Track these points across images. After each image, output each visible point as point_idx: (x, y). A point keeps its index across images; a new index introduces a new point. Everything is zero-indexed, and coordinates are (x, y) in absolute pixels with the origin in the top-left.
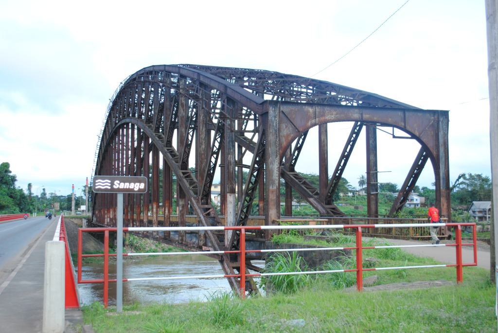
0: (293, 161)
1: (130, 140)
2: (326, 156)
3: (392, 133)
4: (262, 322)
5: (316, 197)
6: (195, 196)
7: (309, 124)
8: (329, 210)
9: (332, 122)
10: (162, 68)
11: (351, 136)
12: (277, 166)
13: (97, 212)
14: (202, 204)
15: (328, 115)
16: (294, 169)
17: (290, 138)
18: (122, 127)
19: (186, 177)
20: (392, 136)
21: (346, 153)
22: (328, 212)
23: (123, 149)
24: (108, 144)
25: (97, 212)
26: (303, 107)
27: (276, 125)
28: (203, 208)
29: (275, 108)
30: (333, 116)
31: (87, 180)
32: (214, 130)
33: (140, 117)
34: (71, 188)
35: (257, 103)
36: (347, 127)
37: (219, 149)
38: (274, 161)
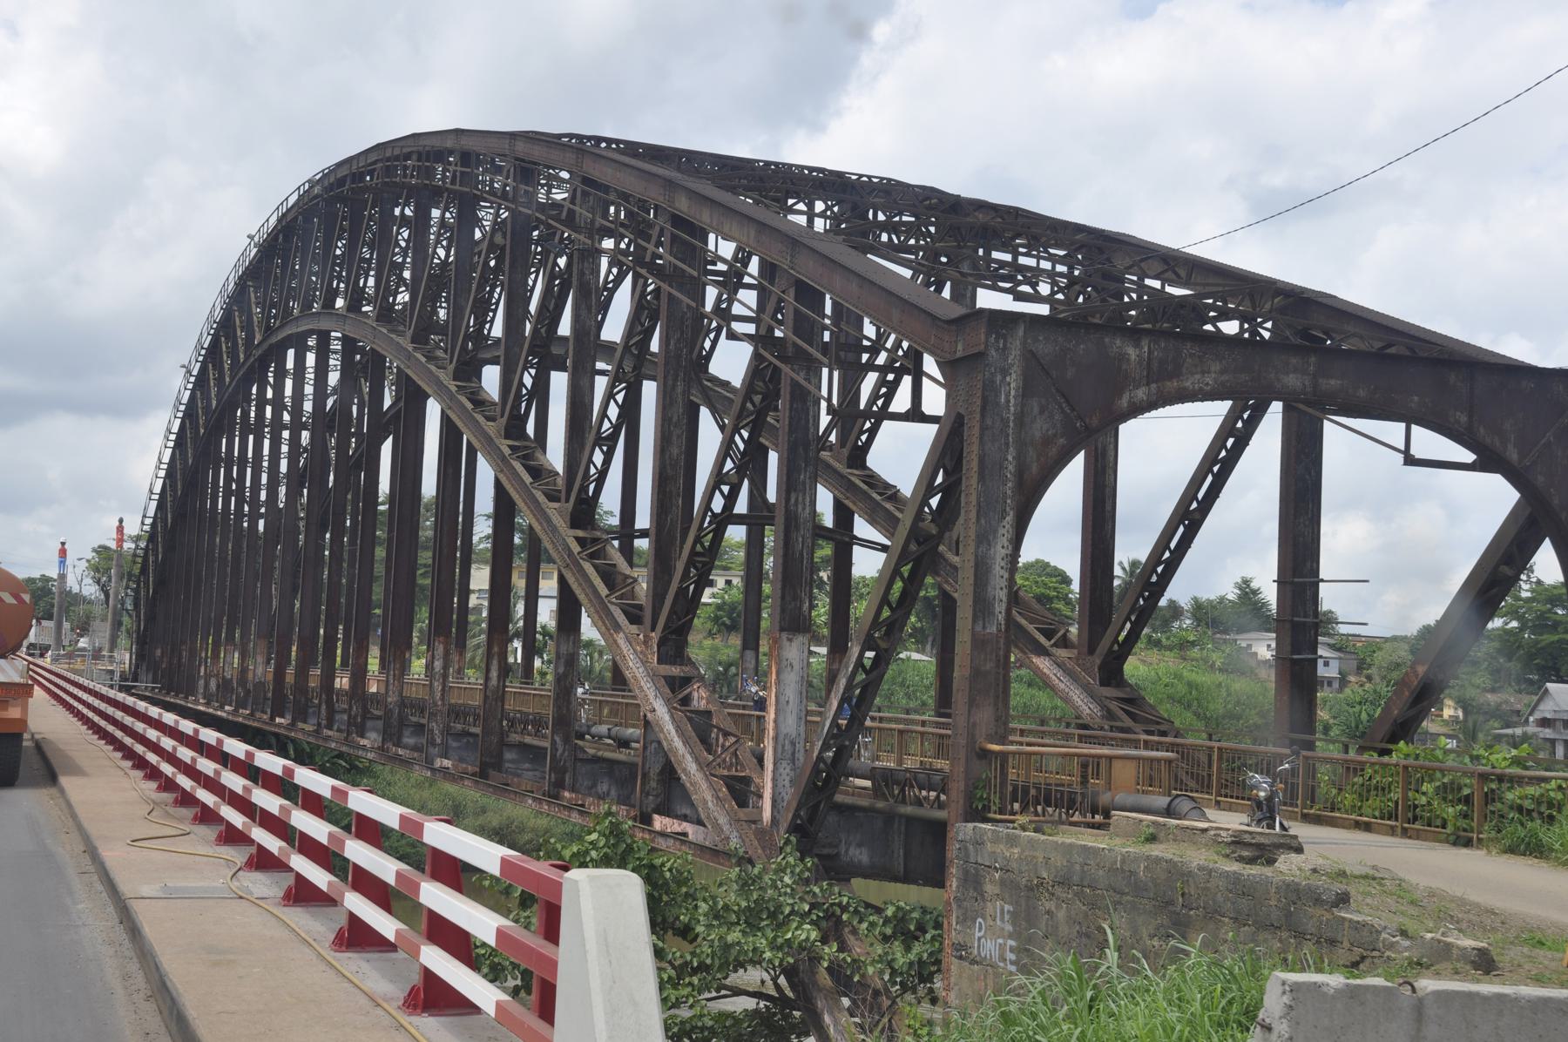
0: (864, 438)
1: (309, 389)
2: (1108, 507)
3: (1403, 449)
4: (1245, 1034)
5: (1062, 653)
6: (634, 629)
7: (1124, 402)
8: (1114, 706)
12: (1004, 552)
13: (159, 652)
15: (1193, 374)
16: (525, 429)
20: (1401, 457)
21: (1194, 505)
22: (1109, 711)
23: (277, 425)
25: (159, 652)
26: (1107, 340)
30: (1209, 379)
31: (120, 529)
32: (653, 378)
33: (354, 305)
34: (56, 559)
35: (934, 318)
37: (616, 428)
38: (995, 532)
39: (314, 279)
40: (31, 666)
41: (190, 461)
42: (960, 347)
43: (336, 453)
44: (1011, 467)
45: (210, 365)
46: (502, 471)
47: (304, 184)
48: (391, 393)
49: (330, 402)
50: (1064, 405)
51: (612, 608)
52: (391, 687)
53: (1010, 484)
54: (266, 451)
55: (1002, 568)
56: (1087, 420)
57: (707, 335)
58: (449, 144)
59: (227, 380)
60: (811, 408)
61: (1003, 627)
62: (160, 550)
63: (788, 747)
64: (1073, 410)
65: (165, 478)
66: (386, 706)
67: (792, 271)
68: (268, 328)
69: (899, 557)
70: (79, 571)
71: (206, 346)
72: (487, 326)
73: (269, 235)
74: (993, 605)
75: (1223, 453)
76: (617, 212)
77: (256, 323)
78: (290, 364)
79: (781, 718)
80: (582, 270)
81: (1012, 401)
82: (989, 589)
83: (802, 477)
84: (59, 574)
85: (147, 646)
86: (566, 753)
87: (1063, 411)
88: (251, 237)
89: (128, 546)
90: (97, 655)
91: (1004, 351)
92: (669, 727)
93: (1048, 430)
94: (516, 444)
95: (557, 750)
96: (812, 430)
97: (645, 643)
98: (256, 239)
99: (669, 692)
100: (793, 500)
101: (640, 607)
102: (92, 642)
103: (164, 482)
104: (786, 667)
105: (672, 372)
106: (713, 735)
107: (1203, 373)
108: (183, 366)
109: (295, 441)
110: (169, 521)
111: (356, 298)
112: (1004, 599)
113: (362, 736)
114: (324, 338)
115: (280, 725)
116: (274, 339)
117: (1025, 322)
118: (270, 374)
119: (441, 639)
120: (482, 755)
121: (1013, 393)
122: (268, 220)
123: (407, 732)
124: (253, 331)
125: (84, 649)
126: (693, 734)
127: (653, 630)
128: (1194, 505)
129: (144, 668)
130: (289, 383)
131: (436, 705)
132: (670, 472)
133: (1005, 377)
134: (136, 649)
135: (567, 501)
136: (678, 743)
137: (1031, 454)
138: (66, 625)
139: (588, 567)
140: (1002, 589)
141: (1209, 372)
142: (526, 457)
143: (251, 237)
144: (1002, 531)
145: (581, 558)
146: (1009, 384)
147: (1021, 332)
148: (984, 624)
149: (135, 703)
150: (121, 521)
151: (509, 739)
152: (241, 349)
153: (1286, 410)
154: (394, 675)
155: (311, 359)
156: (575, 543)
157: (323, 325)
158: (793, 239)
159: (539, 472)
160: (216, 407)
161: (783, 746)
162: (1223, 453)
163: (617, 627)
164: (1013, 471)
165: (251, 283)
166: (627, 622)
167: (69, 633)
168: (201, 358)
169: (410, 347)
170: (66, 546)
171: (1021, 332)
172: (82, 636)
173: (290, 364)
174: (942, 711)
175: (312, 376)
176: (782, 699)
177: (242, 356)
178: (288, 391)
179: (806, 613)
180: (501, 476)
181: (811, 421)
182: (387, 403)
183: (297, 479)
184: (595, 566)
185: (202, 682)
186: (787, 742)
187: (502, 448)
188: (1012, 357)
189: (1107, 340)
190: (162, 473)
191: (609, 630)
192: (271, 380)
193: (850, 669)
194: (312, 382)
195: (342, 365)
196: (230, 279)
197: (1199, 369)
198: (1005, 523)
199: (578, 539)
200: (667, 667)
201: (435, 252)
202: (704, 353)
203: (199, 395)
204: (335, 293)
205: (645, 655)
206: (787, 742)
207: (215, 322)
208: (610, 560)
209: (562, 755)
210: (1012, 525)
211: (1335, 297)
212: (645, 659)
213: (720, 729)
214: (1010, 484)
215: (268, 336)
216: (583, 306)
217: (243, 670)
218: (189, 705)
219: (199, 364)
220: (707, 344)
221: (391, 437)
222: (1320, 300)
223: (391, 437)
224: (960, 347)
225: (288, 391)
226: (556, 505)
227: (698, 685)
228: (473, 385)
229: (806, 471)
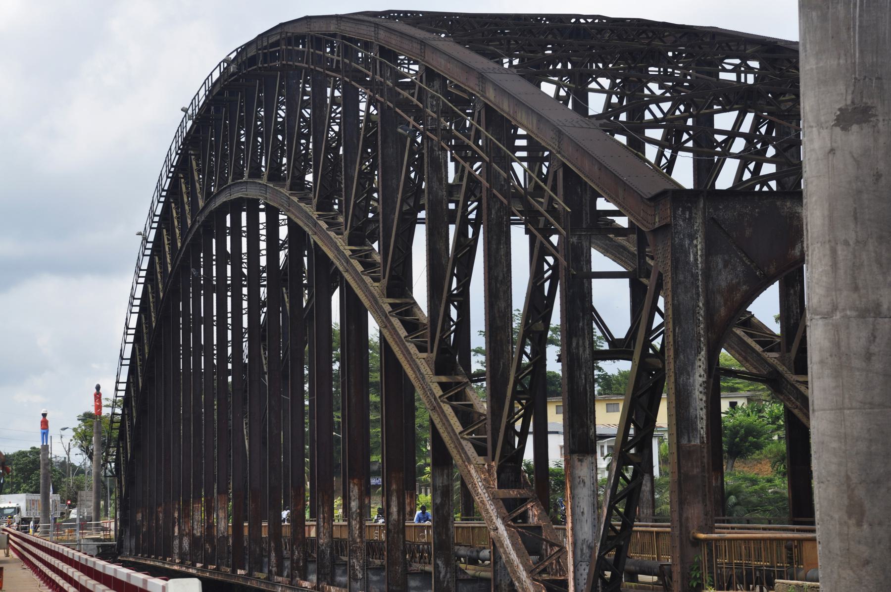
6: (481, 460)
12: (701, 380)
13: (139, 516)
17: (738, 296)
18: (235, 207)
19: (450, 399)
25: (139, 516)
26: (778, 203)
28: (504, 500)
31: (98, 396)
36: (417, 69)
38: (693, 364)
40: (11, 536)
41: (154, 324)
42: (657, 220)
44: (702, 312)
45: (165, 231)
46: (386, 327)
51: (464, 443)
52: (322, 529)
53: (702, 326)
55: (701, 392)
58: (333, 28)
59: (179, 245)
60: (585, 267)
61: (705, 439)
62: (134, 414)
63: (586, 550)
64: (752, 262)
65: (134, 343)
66: (319, 548)
67: (559, 156)
68: (209, 193)
69: (634, 390)
70: (66, 440)
74: (696, 423)
76: (331, 156)
77: (198, 190)
79: (578, 527)
80: (432, 147)
81: (699, 259)
82: (692, 411)
83: (581, 324)
84: (43, 445)
85: (129, 511)
86: (448, 575)
87: (744, 264)
88: (185, 110)
89: (106, 411)
90: (84, 525)
91: (690, 221)
92: (507, 542)
93: (732, 280)
94: (397, 301)
95: (440, 573)
98: (190, 112)
99: (505, 511)
100: (574, 344)
102: (79, 513)
104: (579, 483)
105: (495, 237)
106: (544, 547)
108: (139, 234)
110: (140, 385)
112: (704, 417)
113: (305, 579)
115: (241, 576)
119: (356, 481)
120: (388, 584)
121: (699, 253)
123: (339, 571)
124: (197, 197)
125: (74, 520)
126: (523, 546)
127: (493, 460)
129: (128, 534)
131: (356, 543)
133: (692, 241)
134: (120, 515)
135: (432, 352)
136: (513, 556)
137: (719, 299)
138: (54, 497)
139: (447, 409)
140: (701, 409)
143: (185, 110)
144: (698, 363)
146: (696, 246)
148: (689, 437)
149: (145, 582)
150: (98, 388)
151: (412, 568)
152: (189, 217)
154: (324, 518)
156: (439, 388)
159: (412, 326)
161: (582, 550)
165: (192, 152)
166: (475, 454)
167: (59, 505)
168: (155, 225)
169: (315, 215)
170: (47, 418)
172: (74, 507)
174: (796, 519)
176: (578, 511)
177: (189, 222)
180: (385, 331)
184: (453, 407)
185: (176, 542)
186: (584, 547)
187: (384, 306)
188: (697, 224)
189: (778, 203)
190: (131, 339)
191: (464, 462)
198: (700, 357)
199: (441, 384)
200: (506, 491)
201: (330, 126)
203: (157, 260)
206: (584, 547)
208: (469, 401)
209: (445, 577)
210: (705, 358)
213: (547, 541)
214: (702, 326)
216: (435, 179)
217: (210, 527)
218: (167, 566)
224: (657, 220)
226: (425, 355)
227: (532, 504)
228: (366, 248)
229: (583, 319)
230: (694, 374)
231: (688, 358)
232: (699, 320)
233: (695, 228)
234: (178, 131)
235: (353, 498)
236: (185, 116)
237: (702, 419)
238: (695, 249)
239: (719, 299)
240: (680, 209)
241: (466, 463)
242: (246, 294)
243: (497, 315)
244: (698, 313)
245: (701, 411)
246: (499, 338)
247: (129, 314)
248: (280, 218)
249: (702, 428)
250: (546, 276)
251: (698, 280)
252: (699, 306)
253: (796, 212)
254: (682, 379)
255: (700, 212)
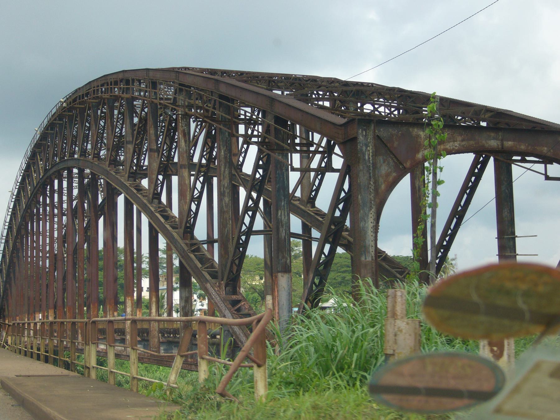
0: (313, 194)
1: (65, 198)
3: (544, 173)
6: (214, 281)
9: (455, 153)
10: (121, 76)
11: (468, 179)
12: (372, 225)
14: (226, 294)
15: (449, 142)
20: (543, 177)
21: (460, 208)
24: (33, 201)
26: (411, 129)
27: (369, 158)
29: (365, 130)
30: (456, 144)
38: (368, 216)
39: (65, 145)
43: (78, 226)
47: (58, 104)
48: (101, 196)
49: (75, 203)
50: (394, 158)
53: (372, 195)
54: (48, 228)
55: (372, 232)
56: (405, 165)
57: (241, 155)
60: (285, 172)
61: (374, 258)
71: (19, 181)
72: (142, 161)
73: (44, 128)
74: (369, 248)
75: (470, 184)
78: (56, 187)
82: (367, 242)
87: (394, 161)
93: (388, 170)
96: (286, 182)
97: (219, 286)
101: (217, 272)
103: (5, 244)
107: (454, 141)
109: (60, 220)
111: (84, 152)
114: (70, 173)
116: (48, 174)
117: (374, 123)
118: (48, 192)
119: (129, 298)
121: (371, 154)
122: (43, 122)
127: (222, 280)
128: (460, 208)
130: (56, 196)
132: (225, 209)
133: (367, 148)
135: (181, 228)
140: (372, 241)
141: (456, 141)
142: (161, 211)
144: (370, 216)
145: (188, 252)
146: (369, 151)
147: (372, 127)
148: (365, 257)
153: (495, 160)
155: (65, 184)
157: (70, 164)
158: (272, 98)
160: (25, 208)
162: (470, 184)
163: (207, 281)
164: (373, 188)
166: (210, 278)
168: (17, 187)
171: (372, 127)
173: (56, 187)
175: (66, 192)
178: (56, 200)
179: (289, 264)
181: (285, 178)
182: (100, 200)
183: (63, 239)
184: (195, 255)
192: (48, 195)
193: (309, 285)
194: (66, 195)
195: (78, 186)
196: (28, 150)
197: (452, 140)
198: (371, 212)
202: (240, 163)
204: (74, 153)
205: (220, 292)
207: (23, 170)
211: (512, 111)
212: (219, 293)
215: (46, 173)
219: (17, 190)
220: (241, 159)
221: (103, 216)
222: (505, 113)
223: (103, 216)
225: (56, 200)
230: (368, 221)
231: (365, 212)
232: (371, 191)
233: (368, 141)
234: (32, 141)
235: (128, 307)
236: (36, 133)
237: (372, 246)
238: (368, 152)
239: (381, 180)
240: (361, 130)
241: (204, 283)
242: (57, 221)
243: (224, 205)
244: (370, 188)
245: (371, 242)
246: (225, 217)
247: (3, 229)
248: (74, 185)
249: (372, 251)
250: (192, 216)
251: (370, 169)
252: (370, 184)
253: (419, 135)
254: (362, 224)
255: (371, 132)
